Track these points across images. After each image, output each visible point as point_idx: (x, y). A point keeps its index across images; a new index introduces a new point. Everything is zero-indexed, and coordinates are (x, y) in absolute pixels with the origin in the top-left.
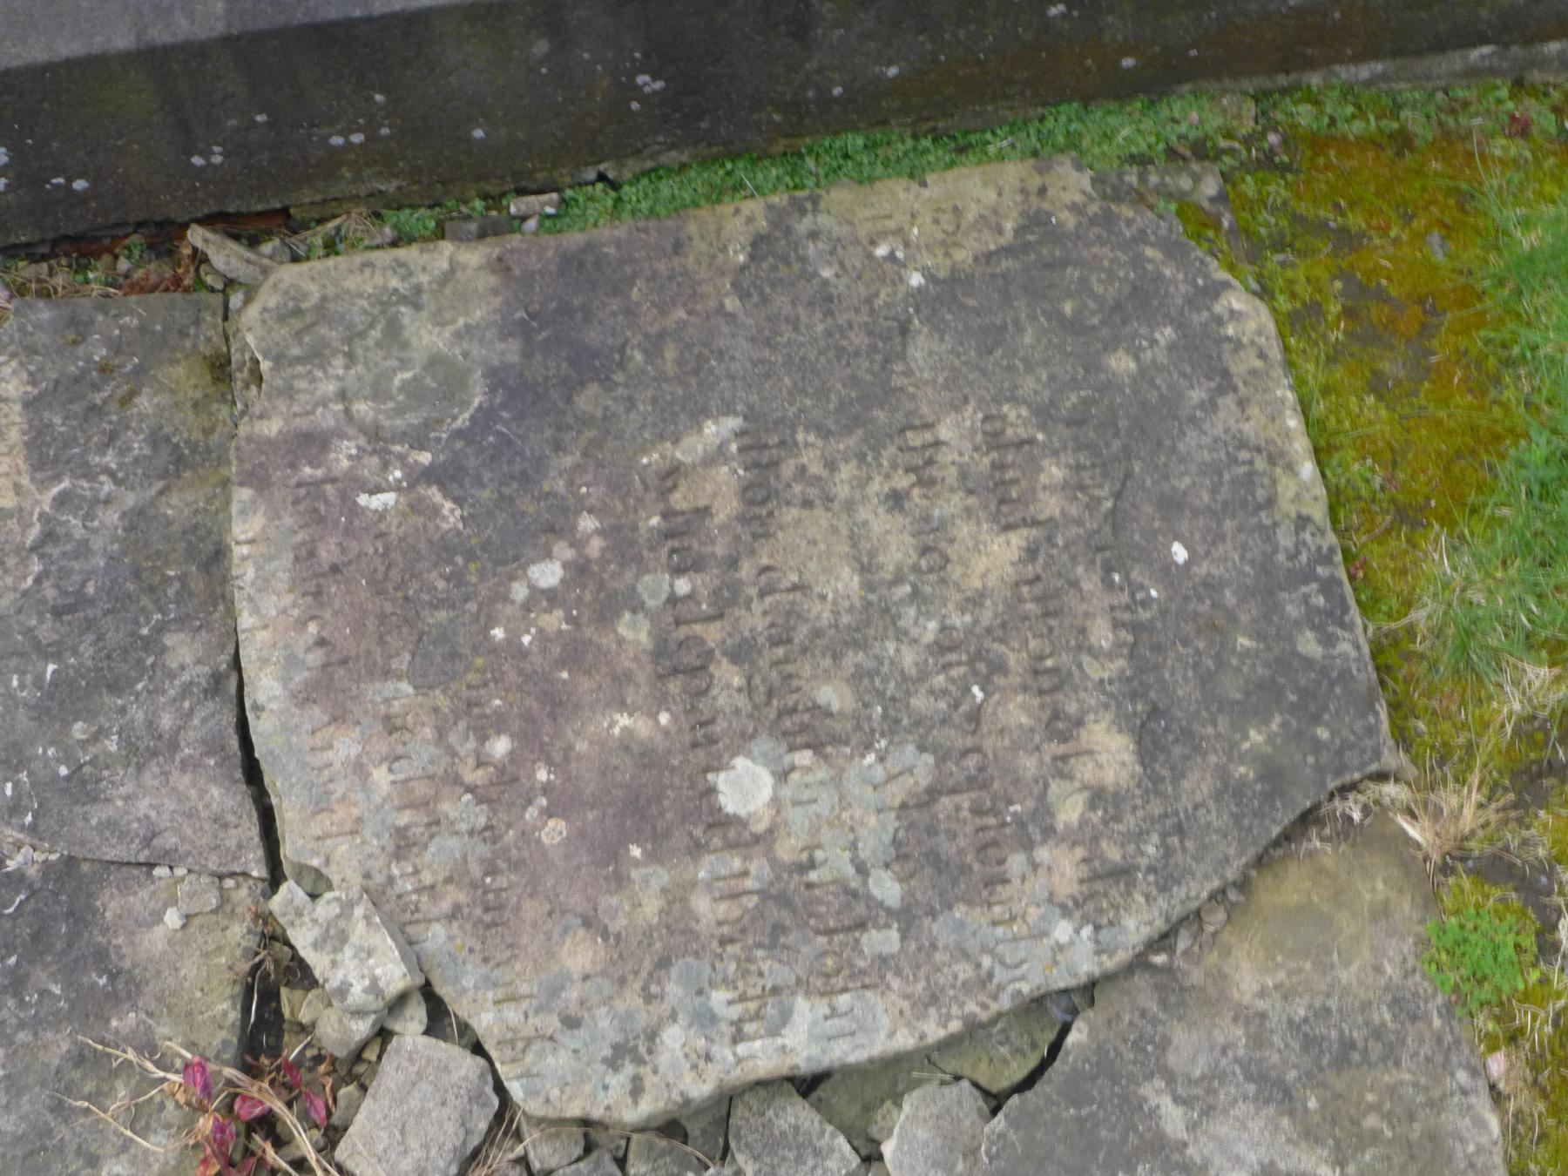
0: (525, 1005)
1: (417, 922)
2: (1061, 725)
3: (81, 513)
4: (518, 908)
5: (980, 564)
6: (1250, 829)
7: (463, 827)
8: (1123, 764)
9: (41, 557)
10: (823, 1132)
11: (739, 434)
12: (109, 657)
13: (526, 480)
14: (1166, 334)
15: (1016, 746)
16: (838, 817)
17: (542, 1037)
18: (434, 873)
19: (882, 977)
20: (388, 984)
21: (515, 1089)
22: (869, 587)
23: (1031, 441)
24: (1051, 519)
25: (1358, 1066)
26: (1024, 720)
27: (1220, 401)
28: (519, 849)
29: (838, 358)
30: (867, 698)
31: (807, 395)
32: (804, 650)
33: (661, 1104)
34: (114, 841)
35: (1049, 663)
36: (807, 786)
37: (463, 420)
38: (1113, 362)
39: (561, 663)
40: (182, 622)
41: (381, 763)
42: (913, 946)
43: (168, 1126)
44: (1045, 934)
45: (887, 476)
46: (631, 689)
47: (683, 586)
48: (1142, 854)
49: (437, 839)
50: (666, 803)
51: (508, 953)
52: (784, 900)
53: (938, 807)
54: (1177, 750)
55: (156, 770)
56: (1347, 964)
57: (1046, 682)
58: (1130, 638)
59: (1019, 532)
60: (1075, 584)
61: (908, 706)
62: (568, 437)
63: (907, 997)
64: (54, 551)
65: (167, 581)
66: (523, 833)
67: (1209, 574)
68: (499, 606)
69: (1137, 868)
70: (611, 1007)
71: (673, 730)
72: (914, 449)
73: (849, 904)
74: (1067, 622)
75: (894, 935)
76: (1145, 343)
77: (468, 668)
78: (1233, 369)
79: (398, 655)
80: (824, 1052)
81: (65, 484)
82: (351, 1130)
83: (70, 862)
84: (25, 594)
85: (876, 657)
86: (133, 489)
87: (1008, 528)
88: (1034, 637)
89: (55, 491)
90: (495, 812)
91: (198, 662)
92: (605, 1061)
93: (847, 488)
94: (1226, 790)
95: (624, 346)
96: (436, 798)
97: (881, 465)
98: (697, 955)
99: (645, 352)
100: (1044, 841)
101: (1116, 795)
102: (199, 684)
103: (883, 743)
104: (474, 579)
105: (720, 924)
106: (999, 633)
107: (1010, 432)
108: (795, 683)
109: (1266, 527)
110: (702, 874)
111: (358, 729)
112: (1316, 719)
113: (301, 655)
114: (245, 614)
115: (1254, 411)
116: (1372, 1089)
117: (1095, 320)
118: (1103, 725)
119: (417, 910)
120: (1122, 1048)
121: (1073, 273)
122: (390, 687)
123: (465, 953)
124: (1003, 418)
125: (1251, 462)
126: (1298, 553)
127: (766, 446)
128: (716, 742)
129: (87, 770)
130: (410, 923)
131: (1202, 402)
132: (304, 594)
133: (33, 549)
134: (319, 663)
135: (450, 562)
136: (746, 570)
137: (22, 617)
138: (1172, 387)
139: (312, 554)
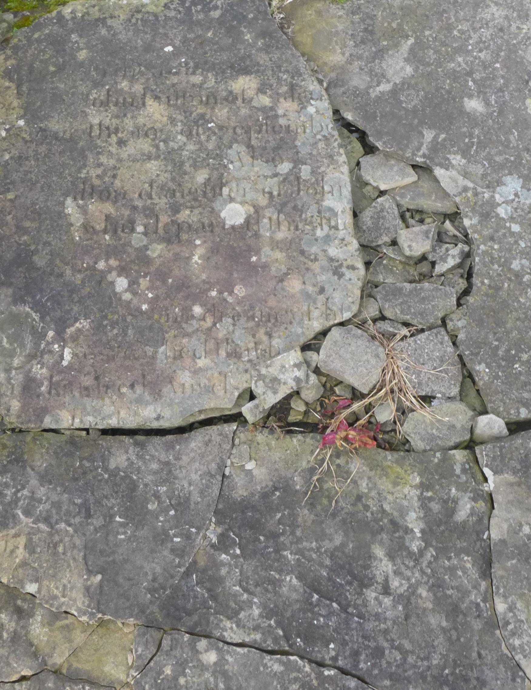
0: (312, 308)
1: (270, 351)
2: (230, 99)
3: (37, 505)
4: (271, 308)
5: (157, 116)
6: (283, 45)
7: (231, 328)
8: (250, 80)
9: (57, 523)
10: (374, 207)
11: (75, 199)
12: (116, 492)
13: (73, 290)
14: (74, 37)
15: (236, 115)
16: (253, 181)
17: (327, 303)
18: (249, 342)
19: (320, 173)
20: (298, 359)
21: (347, 315)
22: (157, 157)
23: (108, 91)
24: (144, 89)
25: (373, 27)
26: (226, 111)
27: (108, 24)
28: (245, 305)
29: (49, 157)
30: (205, 164)
31: (63, 172)
32: (180, 185)
33: (359, 259)
34: (210, 491)
35: (204, 99)
36: (238, 191)
37: (36, 316)
38: (81, 58)
39: (164, 282)
40: (104, 459)
41: (196, 363)
42: (309, 161)
43: (347, 463)
44: (311, 116)
45: (110, 145)
46: (182, 254)
47: (140, 229)
48: (286, 79)
49: (235, 340)
50: (235, 245)
51: (289, 314)
52: (284, 205)
53: (255, 145)
54: (248, 63)
55: (178, 471)
56: (336, 26)
57: (212, 101)
58: (200, 70)
59: (146, 101)
60: (174, 85)
61: (212, 150)
62: (56, 270)
63: (329, 166)
64: (55, 517)
65: (81, 465)
66: (238, 303)
67: (180, 41)
68: (132, 306)
69: (291, 82)
70: (318, 274)
71: (204, 239)
72: (100, 134)
73: (289, 182)
74: (189, 90)
75: (304, 167)
76: (76, 45)
77: (158, 322)
78: (97, 17)
79: (145, 352)
80: (346, 197)
81: (19, 512)
82: (355, 385)
83: (216, 513)
84: (76, 531)
85: (188, 159)
86: (29, 481)
87: (144, 104)
88: (192, 102)
89: (22, 516)
90: (227, 314)
91: (127, 452)
92: (339, 279)
93: (111, 160)
94: (267, 49)
95: (18, 243)
96: (216, 339)
97: (104, 147)
98: (301, 240)
99: (24, 235)
100: (276, 111)
101: (261, 85)
102: (138, 452)
103: (225, 161)
104: (116, 317)
105: (289, 230)
106: (188, 114)
107: (102, 98)
108: (193, 190)
109: (165, 19)
110: (268, 234)
111: (177, 371)
112: (245, 17)
113: (137, 395)
114: (110, 422)
115: (116, 13)
116: (383, 24)
117: (61, 60)
118: (233, 84)
119: (265, 350)
120: (356, 101)
121: (37, 64)
122: (160, 356)
123: (287, 331)
124: (95, 99)
125: (137, 19)
126: (179, 10)
127: (84, 190)
128: (212, 223)
129: (173, 502)
130: (270, 354)
131: (107, 30)
132: (106, 393)
133: (52, 528)
134: (142, 388)
135: (106, 326)
136: (139, 204)
137: (88, 533)
138: (97, 39)
139: (86, 389)
